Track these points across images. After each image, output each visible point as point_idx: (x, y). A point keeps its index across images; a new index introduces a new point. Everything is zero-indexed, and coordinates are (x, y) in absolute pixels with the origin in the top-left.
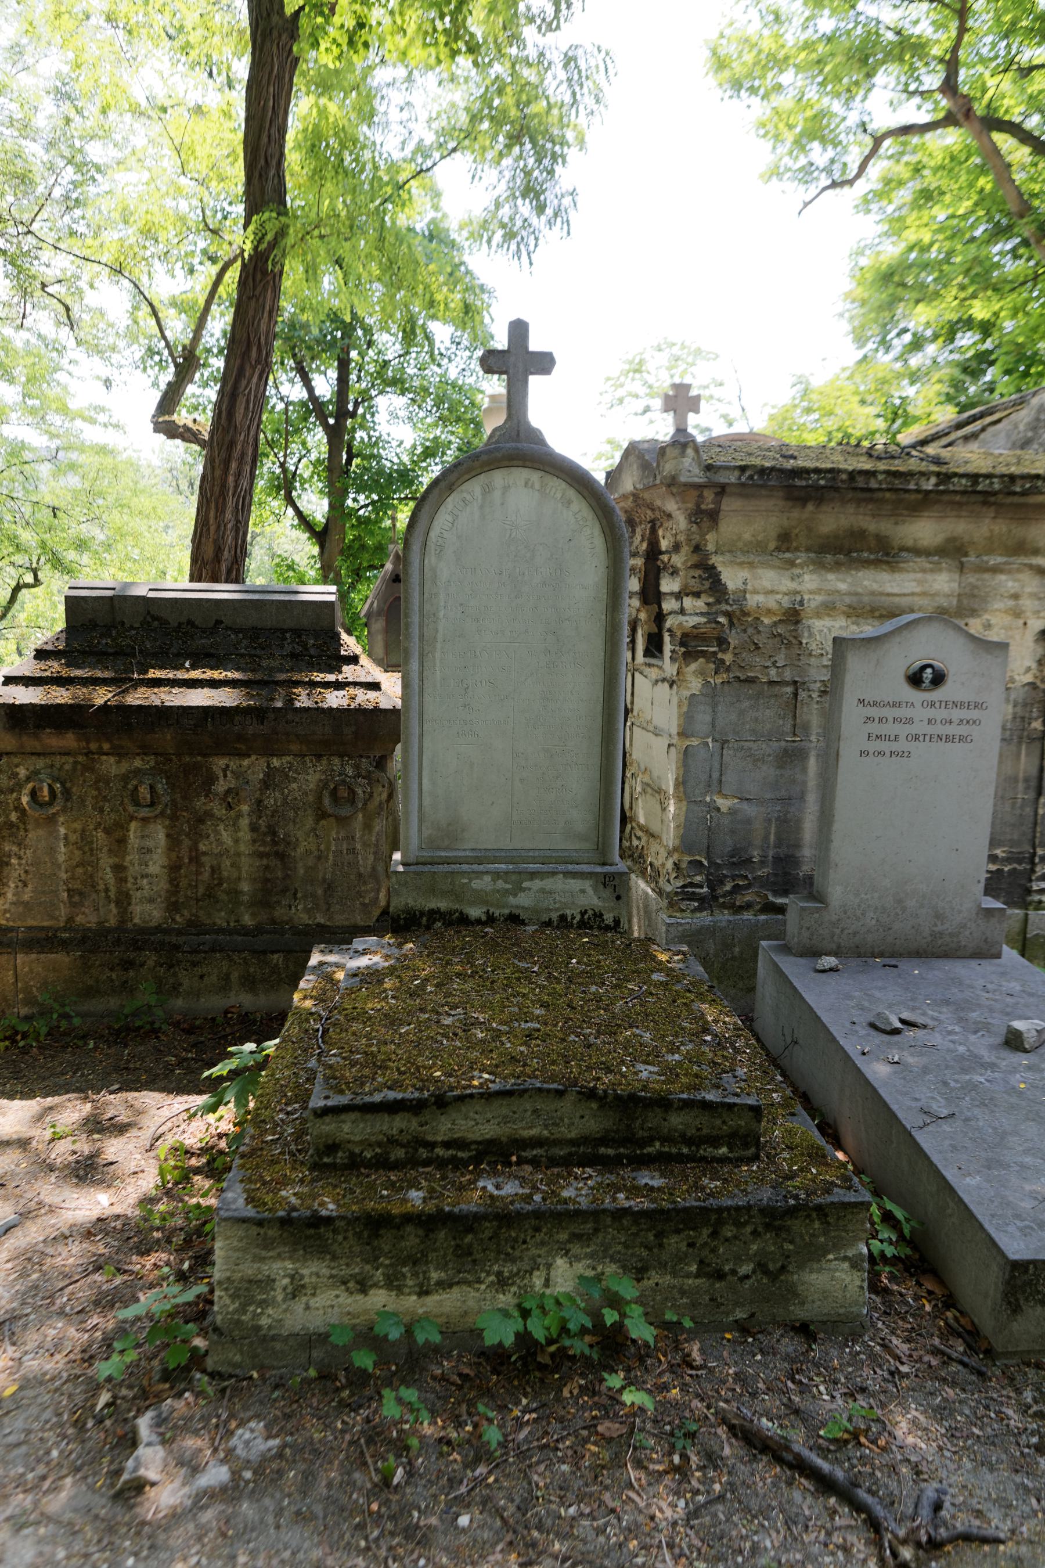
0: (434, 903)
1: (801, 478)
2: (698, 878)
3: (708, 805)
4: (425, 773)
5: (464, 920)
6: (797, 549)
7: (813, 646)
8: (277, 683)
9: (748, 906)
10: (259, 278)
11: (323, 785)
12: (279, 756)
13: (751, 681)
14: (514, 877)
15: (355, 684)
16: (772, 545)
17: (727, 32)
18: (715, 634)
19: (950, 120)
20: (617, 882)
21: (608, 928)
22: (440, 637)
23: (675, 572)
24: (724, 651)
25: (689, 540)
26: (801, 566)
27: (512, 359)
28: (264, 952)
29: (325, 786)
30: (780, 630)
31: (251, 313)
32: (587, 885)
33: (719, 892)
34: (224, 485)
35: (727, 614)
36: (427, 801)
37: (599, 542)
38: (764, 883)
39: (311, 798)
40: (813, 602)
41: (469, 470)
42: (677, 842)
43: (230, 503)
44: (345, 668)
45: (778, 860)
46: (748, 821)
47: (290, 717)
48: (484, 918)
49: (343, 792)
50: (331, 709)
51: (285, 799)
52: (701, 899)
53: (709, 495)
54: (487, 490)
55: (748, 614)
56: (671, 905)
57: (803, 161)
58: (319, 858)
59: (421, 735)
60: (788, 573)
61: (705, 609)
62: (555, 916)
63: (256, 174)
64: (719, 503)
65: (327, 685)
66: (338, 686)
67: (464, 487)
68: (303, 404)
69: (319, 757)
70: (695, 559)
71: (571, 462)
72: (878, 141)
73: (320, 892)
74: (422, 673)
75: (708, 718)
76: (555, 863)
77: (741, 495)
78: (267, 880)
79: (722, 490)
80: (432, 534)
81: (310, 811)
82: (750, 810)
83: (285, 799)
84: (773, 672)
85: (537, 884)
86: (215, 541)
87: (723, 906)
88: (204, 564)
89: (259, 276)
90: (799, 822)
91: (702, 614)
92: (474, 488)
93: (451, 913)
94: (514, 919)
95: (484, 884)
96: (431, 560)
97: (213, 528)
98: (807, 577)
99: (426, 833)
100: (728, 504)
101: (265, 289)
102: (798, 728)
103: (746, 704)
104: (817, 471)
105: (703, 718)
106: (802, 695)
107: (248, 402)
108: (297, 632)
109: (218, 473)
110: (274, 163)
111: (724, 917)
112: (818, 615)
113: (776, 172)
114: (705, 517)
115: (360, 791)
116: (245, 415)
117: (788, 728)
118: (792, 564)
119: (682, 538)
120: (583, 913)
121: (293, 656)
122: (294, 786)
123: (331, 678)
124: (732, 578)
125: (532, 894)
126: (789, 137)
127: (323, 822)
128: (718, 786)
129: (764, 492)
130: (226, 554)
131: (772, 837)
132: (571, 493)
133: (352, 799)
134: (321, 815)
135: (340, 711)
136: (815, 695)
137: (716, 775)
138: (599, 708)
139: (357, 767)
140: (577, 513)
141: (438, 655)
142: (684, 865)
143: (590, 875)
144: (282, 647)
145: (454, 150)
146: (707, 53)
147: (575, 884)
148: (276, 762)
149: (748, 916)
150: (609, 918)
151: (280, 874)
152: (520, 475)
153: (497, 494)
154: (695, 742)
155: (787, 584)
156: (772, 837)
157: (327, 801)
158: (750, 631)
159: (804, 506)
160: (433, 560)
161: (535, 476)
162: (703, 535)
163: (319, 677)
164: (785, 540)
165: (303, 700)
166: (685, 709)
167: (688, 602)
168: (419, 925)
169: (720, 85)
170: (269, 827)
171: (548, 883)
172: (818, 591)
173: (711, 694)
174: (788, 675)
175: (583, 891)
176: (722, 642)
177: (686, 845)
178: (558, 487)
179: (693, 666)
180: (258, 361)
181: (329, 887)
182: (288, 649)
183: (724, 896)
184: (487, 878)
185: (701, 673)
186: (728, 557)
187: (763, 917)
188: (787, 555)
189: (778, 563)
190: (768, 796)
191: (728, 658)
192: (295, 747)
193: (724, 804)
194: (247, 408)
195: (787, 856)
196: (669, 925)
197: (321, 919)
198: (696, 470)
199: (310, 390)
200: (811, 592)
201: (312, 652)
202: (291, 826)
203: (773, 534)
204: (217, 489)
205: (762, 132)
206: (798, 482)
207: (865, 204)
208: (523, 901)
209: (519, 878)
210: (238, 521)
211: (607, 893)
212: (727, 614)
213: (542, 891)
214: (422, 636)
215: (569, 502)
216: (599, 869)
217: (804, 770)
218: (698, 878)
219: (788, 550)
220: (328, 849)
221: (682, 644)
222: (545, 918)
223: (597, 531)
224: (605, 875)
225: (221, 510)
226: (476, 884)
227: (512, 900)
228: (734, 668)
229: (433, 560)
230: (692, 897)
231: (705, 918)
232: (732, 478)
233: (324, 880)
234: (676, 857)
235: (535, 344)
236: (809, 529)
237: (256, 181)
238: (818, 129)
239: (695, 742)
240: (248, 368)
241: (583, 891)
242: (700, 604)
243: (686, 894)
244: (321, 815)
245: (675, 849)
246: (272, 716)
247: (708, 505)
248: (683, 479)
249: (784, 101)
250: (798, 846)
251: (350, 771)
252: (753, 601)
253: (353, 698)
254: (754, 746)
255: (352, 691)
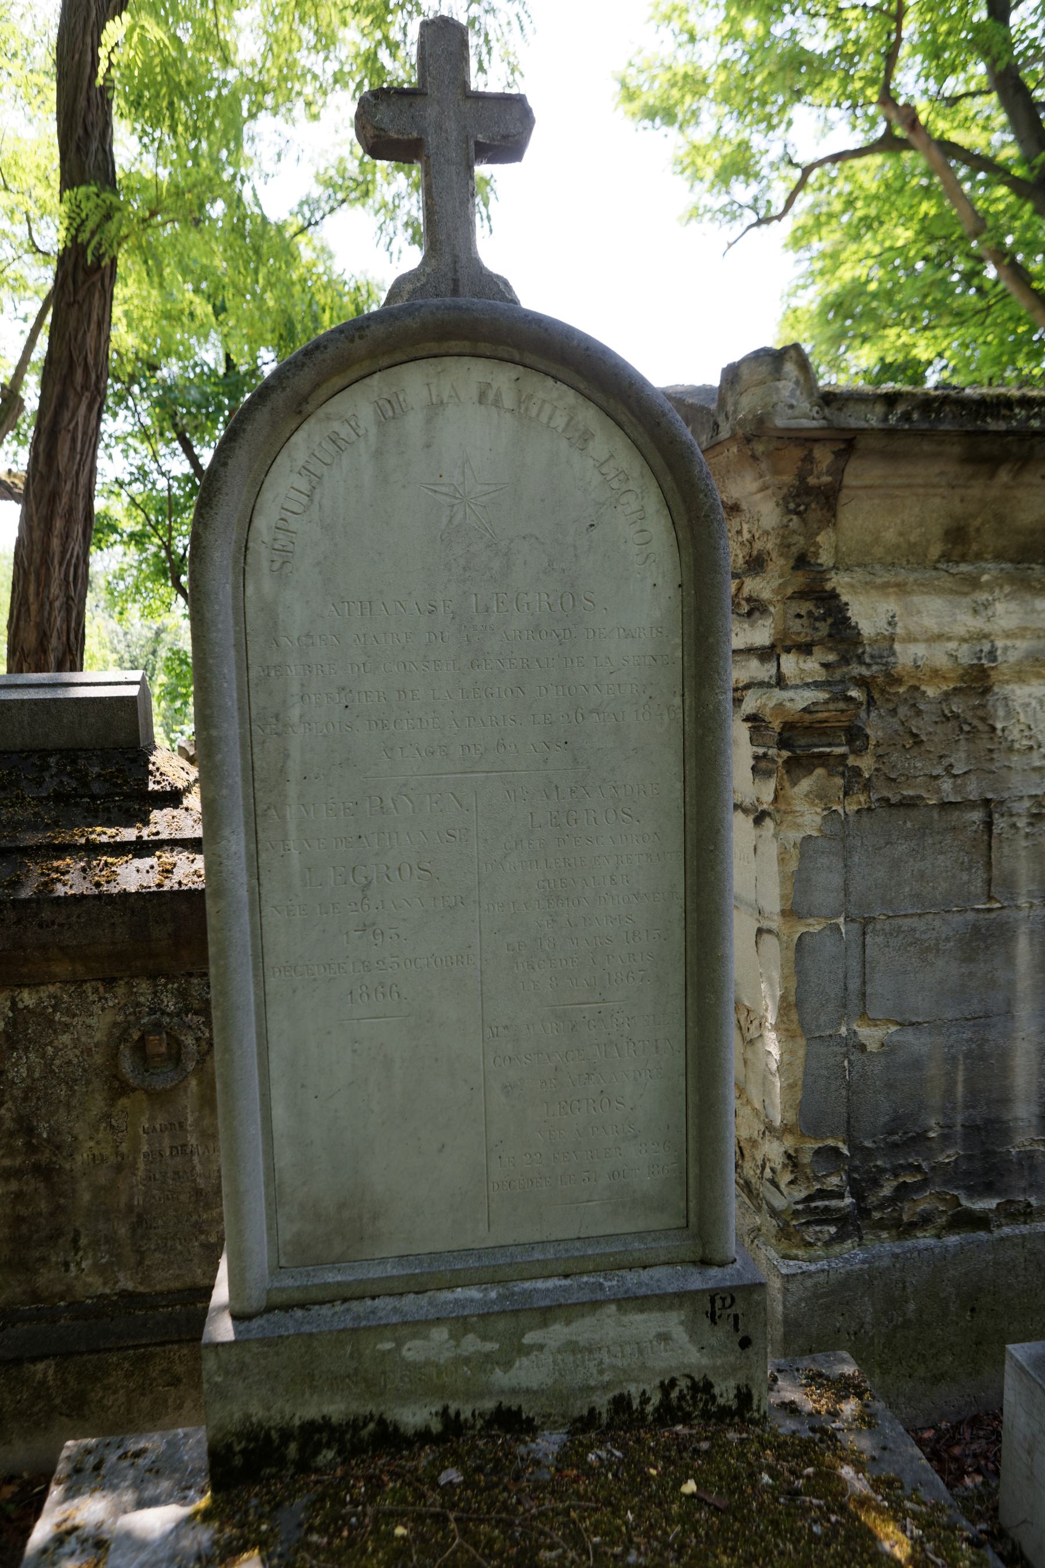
0: (312, 1409)
1: (997, 417)
2: (834, 1181)
3: (844, 1041)
4: (277, 1092)
5: (389, 1438)
6: (979, 556)
7: (1015, 734)
8: (25, 851)
9: (925, 1220)
10: (81, 285)
11: (120, 1035)
12: (34, 983)
13: (909, 804)
14: (502, 1325)
15: (174, 844)
16: (935, 550)
17: (637, 61)
18: (844, 721)
19: (889, 144)
20: (738, 1309)
21: (724, 1413)
22: (294, 767)
23: (756, 609)
24: (858, 752)
25: (785, 546)
26: (990, 587)
27: (432, 112)
28: (18, 1362)
29: (123, 1038)
30: (957, 706)
31: (72, 324)
32: (674, 1322)
33: (872, 1200)
34: (46, 551)
35: (862, 682)
36: (285, 1157)
37: (658, 529)
38: (951, 1175)
39: (98, 1059)
40: (1014, 651)
41: (343, 364)
42: (791, 1117)
43: (57, 574)
44: (156, 815)
45: (972, 1129)
46: (917, 1064)
47: (46, 915)
48: (436, 1426)
49: (158, 1045)
50: (125, 895)
51: (48, 1065)
52: (841, 1220)
53: (824, 457)
54: (390, 413)
55: (899, 681)
56: (784, 1233)
57: (725, 199)
58: (119, 1168)
59: (262, 1004)
60: (967, 601)
61: (821, 675)
62: (602, 1402)
63: (73, 146)
64: (838, 472)
65: (120, 849)
66: (141, 849)
67: (334, 406)
68: (188, 478)
69: (110, 982)
70: (800, 580)
71: (587, 338)
72: (807, 171)
73: (123, 1231)
74: (254, 858)
75: (836, 880)
76: (594, 1274)
77: (890, 456)
78: (20, 1220)
79: (849, 445)
80: (261, 523)
81: (97, 1083)
82: (917, 1043)
83: (48, 1065)
84: (947, 785)
85: (558, 1333)
86: (38, 625)
87: (881, 1225)
88: (24, 656)
89: (81, 276)
90: (1005, 1056)
91: (817, 685)
92: (357, 408)
93: (355, 1425)
94: (510, 1421)
95: (433, 1347)
96: (262, 585)
97: (34, 608)
98: (1000, 607)
99: (288, 1231)
100: (861, 474)
101: (90, 292)
102: (996, 886)
103: (902, 848)
104: (1026, 402)
105: (828, 878)
106: (1000, 823)
107: (74, 440)
108: (70, 754)
109: (37, 535)
110: (97, 133)
111: (885, 1246)
112: (1020, 676)
113: (695, 214)
114: (814, 501)
115: (189, 1041)
116: (72, 458)
117: (978, 886)
118: (973, 583)
119: (770, 544)
120: (666, 1388)
121: (59, 797)
122: (66, 1038)
123: (129, 834)
124: (868, 613)
125: (546, 1358)
126: (709, 174)
127: (124, 1101)
128: (858, 1002)
129: (927, 447)
130: (54, 641)
131: (960, 1089)
132: (589, 416)
133: (176, 1055)
134: (119, 1088)
135: (144, 897)
136: (1021, 823)
137: (854, 984)
138: (677, 911)
139: (182, 994)
140: (602, 466)
141: (292, 812)
142: (806, 1159)
143: (681, 1298)
144: (40, 783)
145: (343, 201)
146: (618, 87)
147: (644, 1324)
148: (27, 998)
149: (924, 1240)
150: (725, 1392)
151: (44, 1206)
152: (467, 377)
153: (414, 423)
154: (815, 926)
155: (966, 622)
156: (960, 1089)
157: (126, 1065)
158: (903, 711)
159: (992, 475)
160: (267, 585)
161: (502, 378)
162: (811, 536)
163: (103, 834)
164: (958, 541)
165: (73, 881)
166: (793, 865)
167: (790, 664)
168: (282, 1462)
169: (634, 114)
170: (19, 1119)
171: (582, 1329)
172: (1021, 632)
173: (839, 834)
174: (973, 790)
175: (664, 1337)
176: (855, 736)
177: (808, 1119)
178: (557, 401)
179: (806, 784)
180: (85, 387)
181: (141, 1222)
182: (50, 785)
183: (881, 1207)
184: (440, 1334)
185: (820, 795)
186: (859, 574)
187: (953, 1239)
188: (964, 568)
189: (947, 582)
190: (949, 1014)
191: (866, 763)
192: (62, 969)
193: (871, 1035)
194: (73, 448)
195: (988, 1122)
196: (788, 1278)
197: (126, 1282)
198: (804, 405)
199: (194, 460)
200: (1008, 635)
201: (96, 788)
202: (62, 1115)
203: (937, 530)
204: (37, 556)
205: (679, 168)
206: (994, 425)
207: (799, 239)
208: (528, 1375)
209: (516, 1318)
210: (69, 598)
211: (720, 1335)
212: (862, 682)
213: (572, 1347)
214: (250, 770)
215: (586, 437)
216: (697, 1281)
217: (1010, 960)
218: (834, 1181)
219: (963, 558)
220: (135, 1150)
221: (783, 743)
222: (579, 1408)
223: (653, 502)
224: (713, 1295)
225: (43, 583)
226: (414, 1351)
227: (500, 1378)
228: (877, 783)
229: (267, 585)
230: (825, 1217)
231: (851, 1255)
232: (873, 417)
233: (130, 1208)
234: (789, 1142)
235: (487, 79)
236: (1000, 518)
237: (72, 155)
238: (739, 165)
239: (815, 926)
240: (71, 395)
241: (664, 1337)
242: (812, 666)
243: (814, 1212)
244: (119, 1088)
245: (787, 1129)
246: (11, 916)
247: (820, 478)
248: (780, 422)
249: (701, 134)
250: (1005, 1101)
251: (170, 1004)
252: (907, 654)
253: (167, 872)
254: (914, 922)
255: (167, 857)
